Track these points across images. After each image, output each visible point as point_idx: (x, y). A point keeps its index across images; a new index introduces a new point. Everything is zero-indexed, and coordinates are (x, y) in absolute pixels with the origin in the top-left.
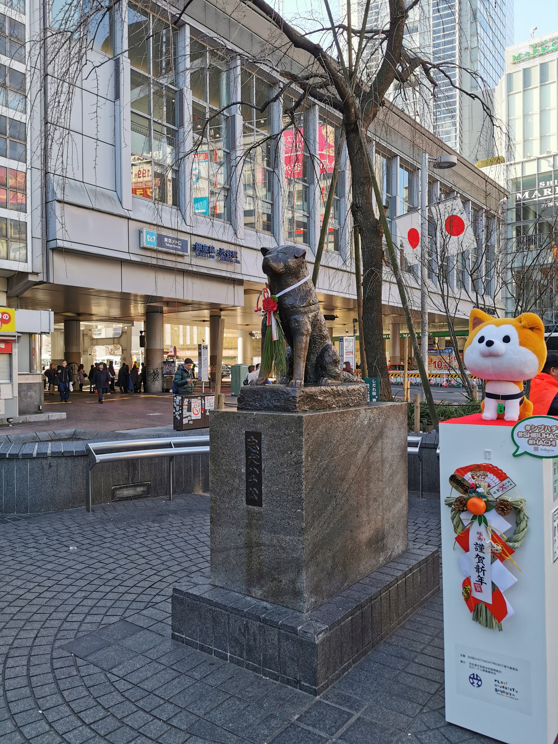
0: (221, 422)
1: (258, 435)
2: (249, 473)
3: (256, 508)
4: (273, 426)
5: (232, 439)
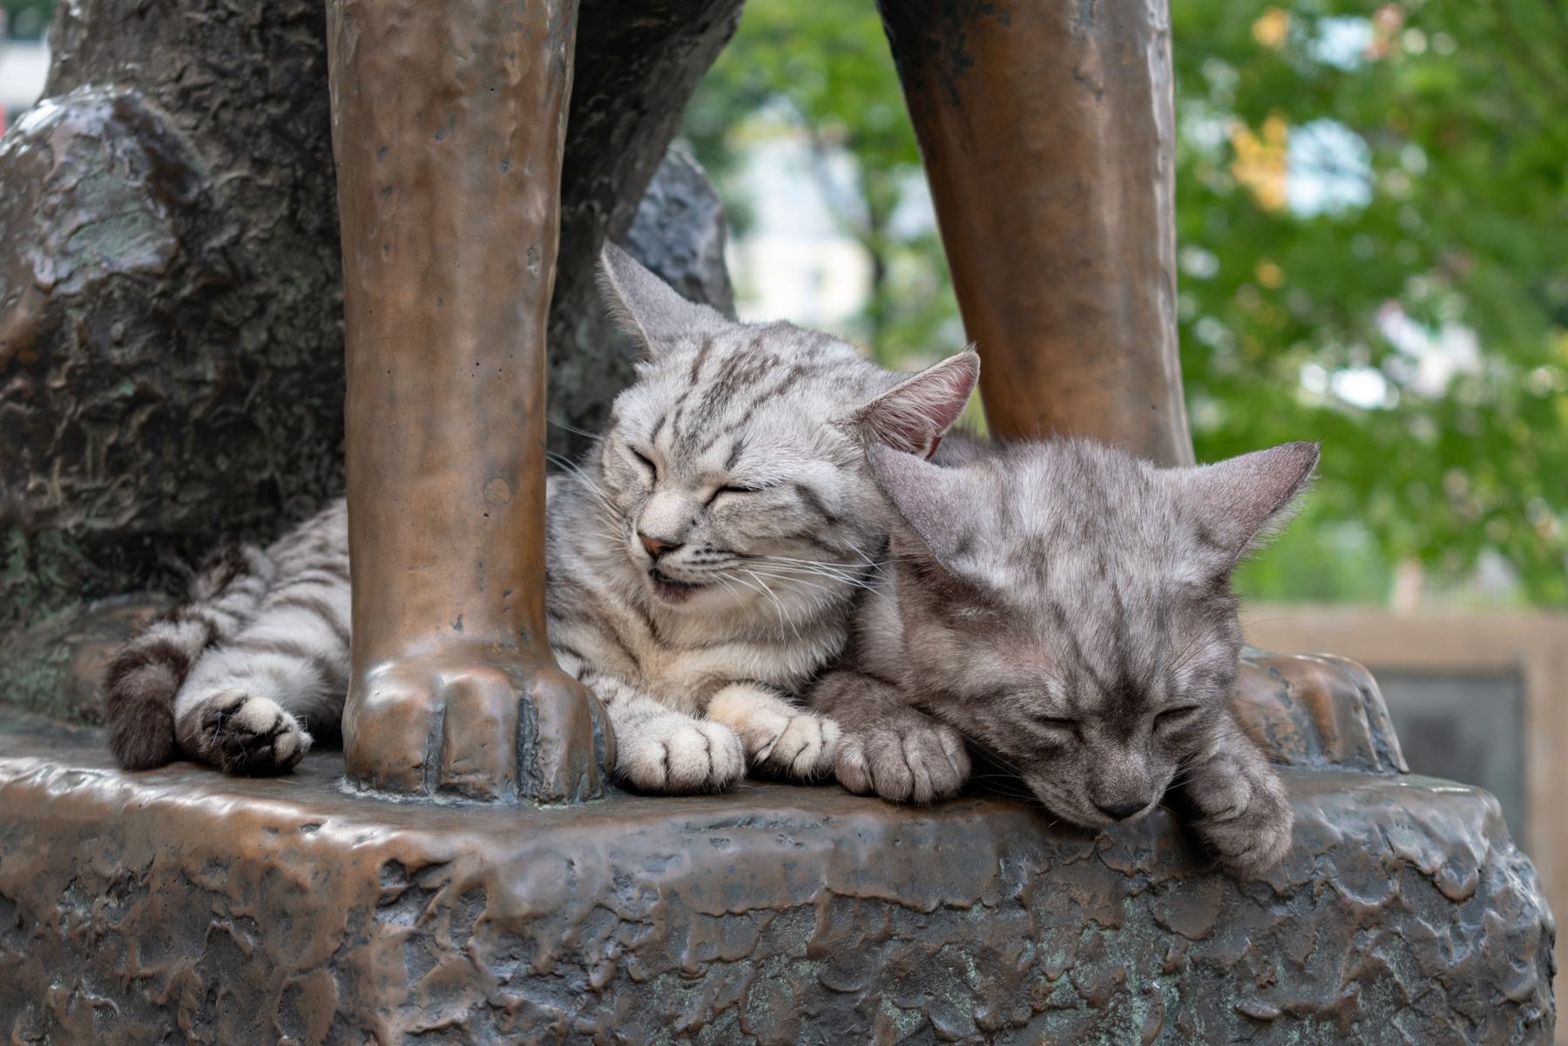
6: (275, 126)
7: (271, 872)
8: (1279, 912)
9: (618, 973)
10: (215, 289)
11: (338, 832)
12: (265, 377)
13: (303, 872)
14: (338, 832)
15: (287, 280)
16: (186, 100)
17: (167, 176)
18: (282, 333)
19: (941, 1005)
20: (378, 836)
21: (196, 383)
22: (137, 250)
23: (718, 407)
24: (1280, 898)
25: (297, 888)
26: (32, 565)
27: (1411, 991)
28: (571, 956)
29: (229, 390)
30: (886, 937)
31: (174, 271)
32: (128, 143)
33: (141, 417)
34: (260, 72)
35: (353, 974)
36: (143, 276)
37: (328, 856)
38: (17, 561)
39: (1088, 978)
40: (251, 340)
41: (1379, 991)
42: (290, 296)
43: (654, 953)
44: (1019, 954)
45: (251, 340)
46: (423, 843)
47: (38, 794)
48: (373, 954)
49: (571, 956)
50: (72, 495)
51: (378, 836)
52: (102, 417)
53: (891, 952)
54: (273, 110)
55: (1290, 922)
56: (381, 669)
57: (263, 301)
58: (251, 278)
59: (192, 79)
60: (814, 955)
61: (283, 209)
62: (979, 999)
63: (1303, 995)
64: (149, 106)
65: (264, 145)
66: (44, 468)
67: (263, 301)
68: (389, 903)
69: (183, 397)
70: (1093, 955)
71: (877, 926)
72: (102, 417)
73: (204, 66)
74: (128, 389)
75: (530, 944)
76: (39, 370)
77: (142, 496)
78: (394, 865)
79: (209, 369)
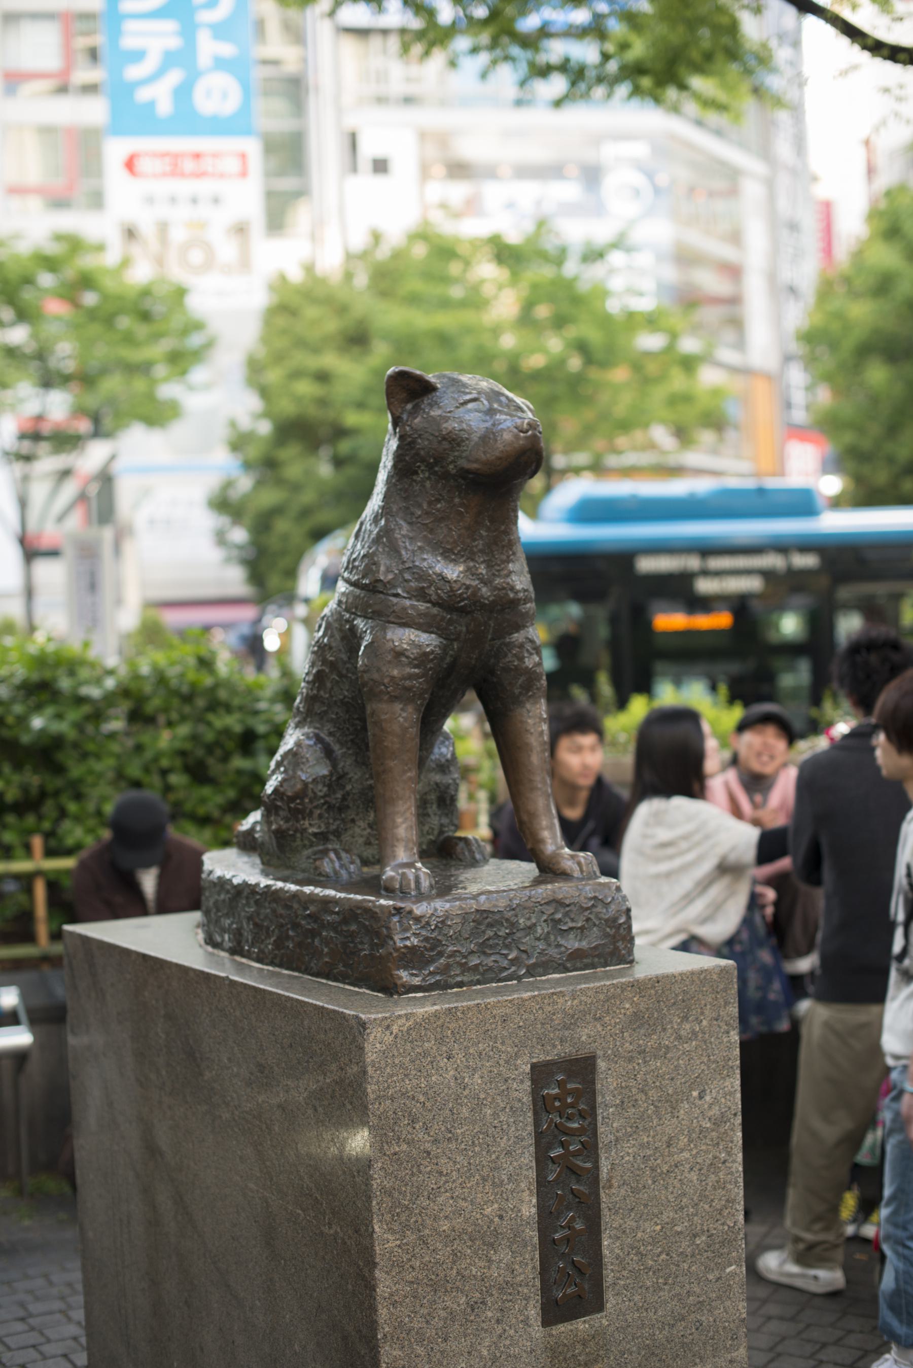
0: (426, 1054)
1: (582, 1068)
2: (546, 1218)
3: (581, 1325)
4: (637, 1020)
5: (481, 1104)
6: (352, 741)
7: (370, 910)
8: (568, 909)
9: (436, 926)
10: (340, 777)
11: (383, 902)
12: (351, 796)
13: (377, 910)
14: (383, 902)
15: (355, 774)
16: (330, 734)
17: (328, 752)
18: (355, 785)
19: (499, 930)
20: (391, 903)
21: (336, 799)
22: (324, 771)
23: (623, 89)
24: (568, 906)
25: (376, 913)
26: (302, 840)
27: (597, 923)
28: (428, 923)
29: (344, 798)
30: (487, 918)
31: (331, 774)
32: (319, 746)
33: (325, 807)
34: (348, 729)
35: (388, 928)
36: (324, 777)
37: (381, 906)
38: (298, 840)
39: (529, 923)
40: (348, 787)
41: (590, 923)
42: (356, 777)
43: (443, 922)
44: (514, 920)
45: (348, 787)
46: (400, 904)
47: (317, 895)
48: (392, 925)
49: (428, 923)
50: (310, 825)
51: (391, 903)
52: (316, 807)
53: (489, 920)
54: (351, 737)
55: (570, 911)
56: (388, 869)
57: (350, 779)
58: (347, 774)
59: (332, 730)
60: (474, 921)
61: (354, 758)
62: (506, 928)
63: (574, 925)
64: (322, 735)
65: (349, 744)
66: (304, 819)
67: (350, 779)
68: (394, 915)
69: (334, 802)
70: (529, 919)
71: (485, 915)
72: (316, 807)
73: (335, 727)
74: (322, 801)
75: (420, 922)
76: (302, 799)
77: (325, 824)
78: (395, 908)
79: (339, 795)
